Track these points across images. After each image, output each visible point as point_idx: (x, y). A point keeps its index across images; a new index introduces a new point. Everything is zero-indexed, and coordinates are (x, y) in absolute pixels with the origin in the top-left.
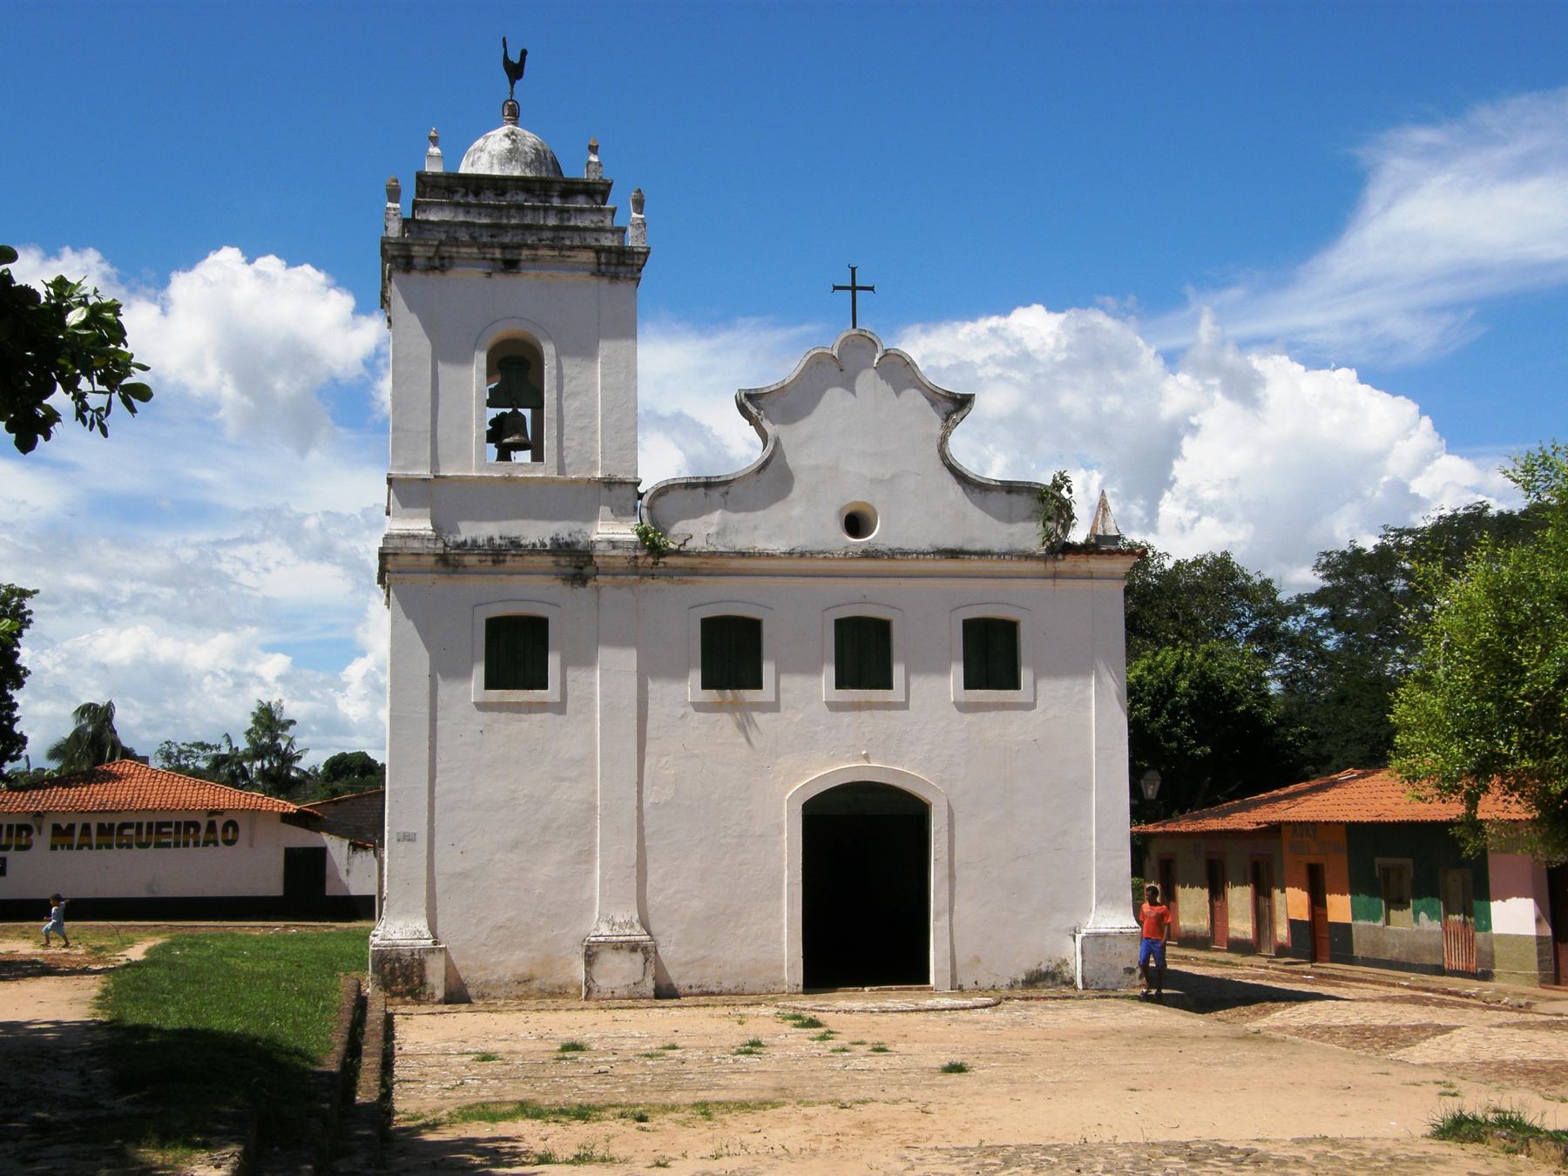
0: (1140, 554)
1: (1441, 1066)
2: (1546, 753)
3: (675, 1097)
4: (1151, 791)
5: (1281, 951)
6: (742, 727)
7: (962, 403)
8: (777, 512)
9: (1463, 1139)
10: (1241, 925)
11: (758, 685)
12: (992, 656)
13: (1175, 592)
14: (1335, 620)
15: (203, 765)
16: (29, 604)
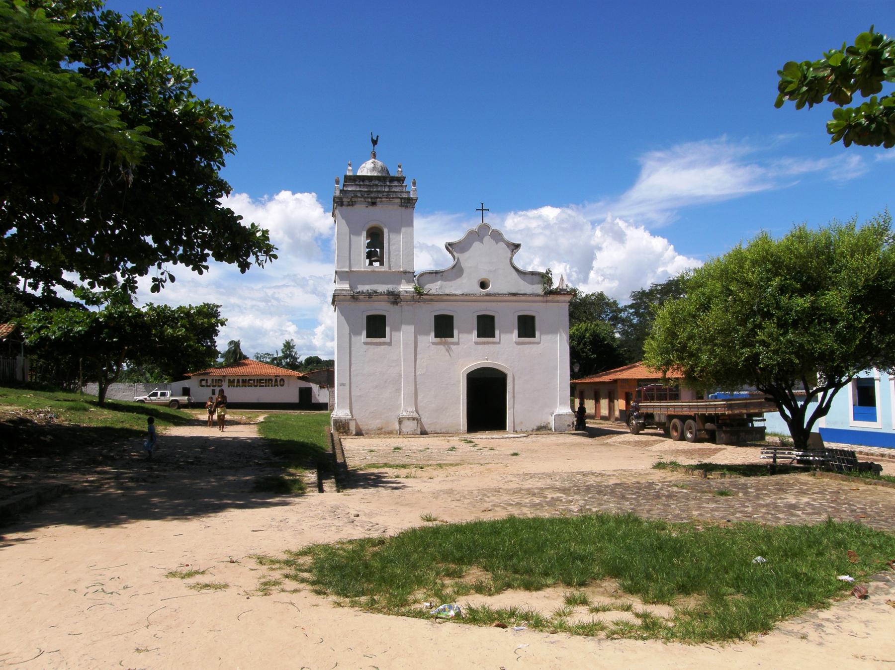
0: (573, 292)
1: (661, 451)
2: (683, 359)
3: (430, 462)
4: (576, 370)
5: (617, 419)
6: (447, 350)
7: (517, 246)
8: (459, 281)
9: (660, 469)
10: (604, 412)
11: (452, 336)
12: (527, 327)
13: (586, 305)
14: (636, 314)
15: (269, 360)
16: (219, 310)
